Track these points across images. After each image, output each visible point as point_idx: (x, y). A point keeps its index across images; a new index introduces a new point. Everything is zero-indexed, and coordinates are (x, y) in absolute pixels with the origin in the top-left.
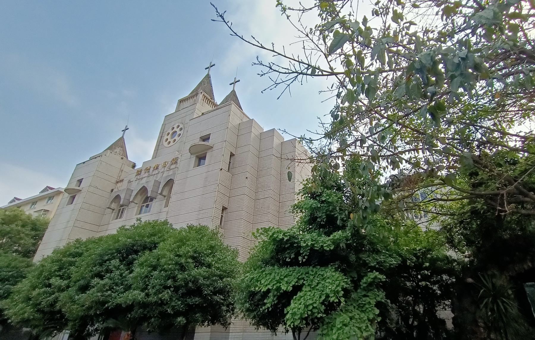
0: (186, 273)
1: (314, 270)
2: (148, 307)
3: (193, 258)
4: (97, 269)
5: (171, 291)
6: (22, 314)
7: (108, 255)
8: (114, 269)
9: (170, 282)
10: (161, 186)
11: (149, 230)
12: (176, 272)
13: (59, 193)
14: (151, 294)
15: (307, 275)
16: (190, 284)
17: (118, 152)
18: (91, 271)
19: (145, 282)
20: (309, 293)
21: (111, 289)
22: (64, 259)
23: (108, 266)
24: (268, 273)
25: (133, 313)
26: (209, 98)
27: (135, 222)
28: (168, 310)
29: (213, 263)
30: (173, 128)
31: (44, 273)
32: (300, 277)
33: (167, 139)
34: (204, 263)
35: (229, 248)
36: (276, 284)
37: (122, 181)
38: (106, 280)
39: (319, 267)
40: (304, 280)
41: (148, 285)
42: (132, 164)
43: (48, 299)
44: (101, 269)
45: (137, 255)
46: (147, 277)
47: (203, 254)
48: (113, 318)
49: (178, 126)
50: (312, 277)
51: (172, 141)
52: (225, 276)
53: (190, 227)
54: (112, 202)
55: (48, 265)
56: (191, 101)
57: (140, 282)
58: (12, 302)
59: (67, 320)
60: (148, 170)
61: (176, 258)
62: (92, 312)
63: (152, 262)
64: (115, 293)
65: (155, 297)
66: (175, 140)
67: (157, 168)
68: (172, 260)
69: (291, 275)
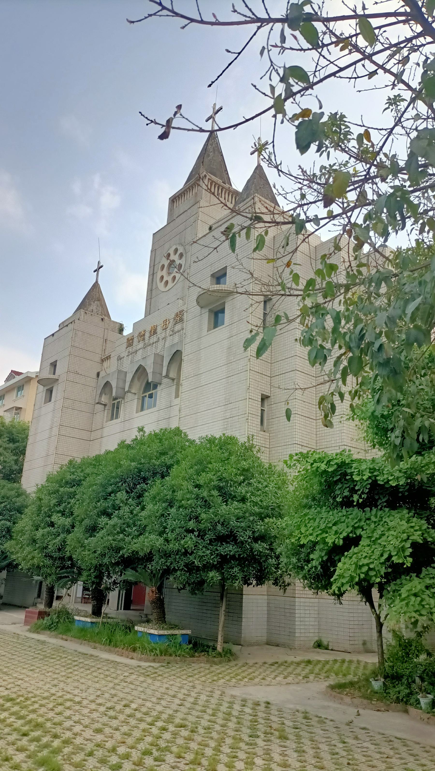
0: (211, 510)
1: (379, 513)
2: (170, 556)
3: (220, 489)
4: (102, 504)
5: (195, 536)
6: (31, 559)
7: (111, 485)
8: (121, 505)
9: (192, 524)
10: (166, 363)
11: (156, 447)
12: (199, 509)
13: (28, 379)
14: (171, 540)
15: (368, 522)
16: (219, 527)
17: (95, 311)
18: (96, 507)
19: (161, 523)
20: (367, 548)
21: (123, 531)
22: (62, 489)
23: (114, 500)
24: (312, 519)
25: (153, 563)
26: (220, 181)
27: (137, 433)
28: (194, 562)
29: (249, 495)
30: (169, 255)
31: (43, 508)
32: (356, 525)
33: (162, 277)
34: (235, 495)
35: (273, 468)
36: (321, 534)
37: (108, 358)
38: (115, 520)
39: (387, 510)
40: (363, 530)
41: (165, 528)
42: (117, 327)
43: (54, 541)
44: (107, 505)
45: (147, 484)
46: (163, 515)
47: (232, 483)
48: (132, 569)
49: (176, 251)
50: (373, 526)
51: (170, 279)
52: (268, 516)
53: (211, 441)
54: (101, 394)
55: (46, 499)
56: (190, 196)
57: (156, 523)
58: (17, 544)
59: (80, 570)
60: (142, 336)
61: (195, 489)
62: (106, 560)
63: (166, 495)
64: (128, 536)
65: (177, 544)
66: (174, 278)
67: (155, 332)
68: (191, 492)
69: (344, 522)
